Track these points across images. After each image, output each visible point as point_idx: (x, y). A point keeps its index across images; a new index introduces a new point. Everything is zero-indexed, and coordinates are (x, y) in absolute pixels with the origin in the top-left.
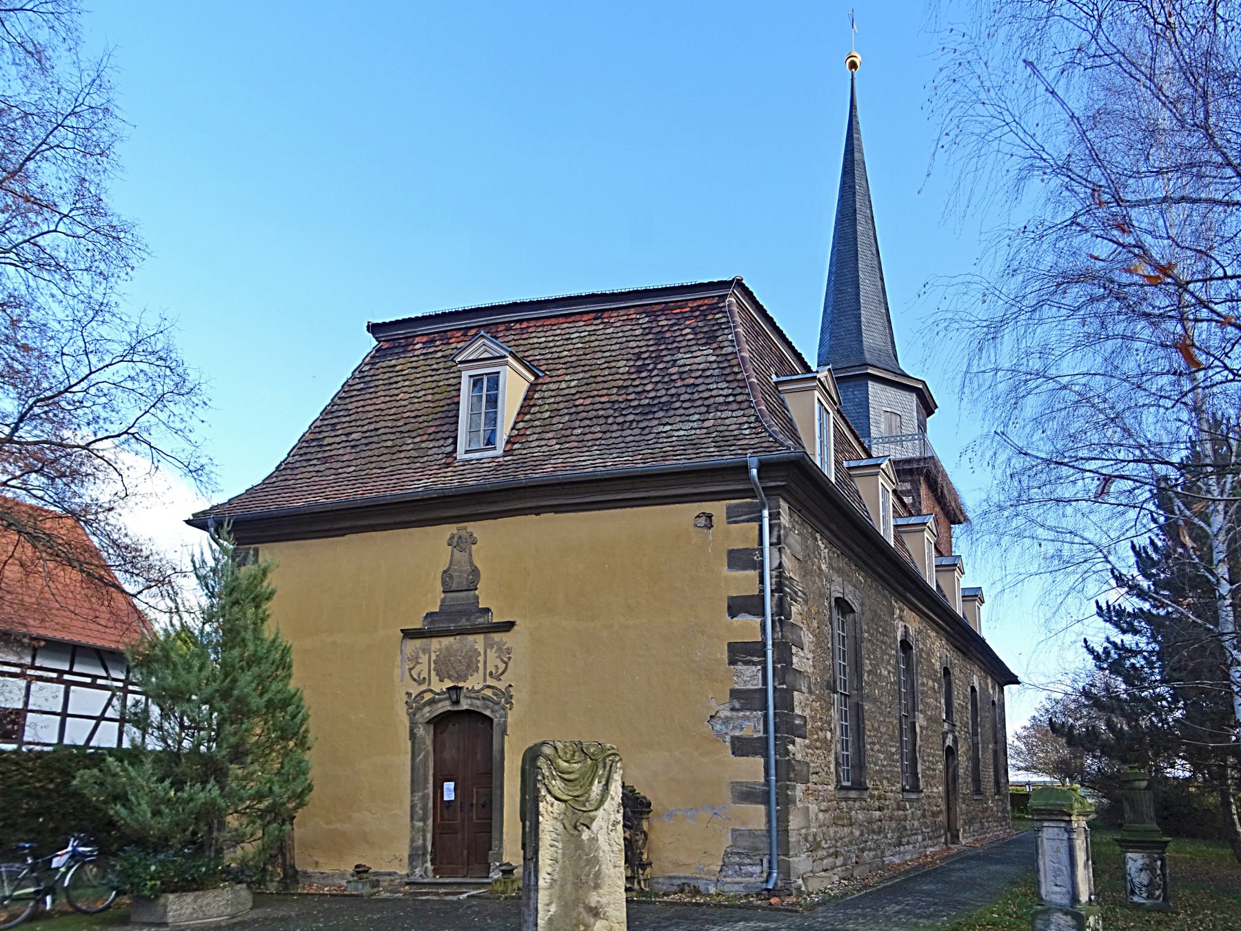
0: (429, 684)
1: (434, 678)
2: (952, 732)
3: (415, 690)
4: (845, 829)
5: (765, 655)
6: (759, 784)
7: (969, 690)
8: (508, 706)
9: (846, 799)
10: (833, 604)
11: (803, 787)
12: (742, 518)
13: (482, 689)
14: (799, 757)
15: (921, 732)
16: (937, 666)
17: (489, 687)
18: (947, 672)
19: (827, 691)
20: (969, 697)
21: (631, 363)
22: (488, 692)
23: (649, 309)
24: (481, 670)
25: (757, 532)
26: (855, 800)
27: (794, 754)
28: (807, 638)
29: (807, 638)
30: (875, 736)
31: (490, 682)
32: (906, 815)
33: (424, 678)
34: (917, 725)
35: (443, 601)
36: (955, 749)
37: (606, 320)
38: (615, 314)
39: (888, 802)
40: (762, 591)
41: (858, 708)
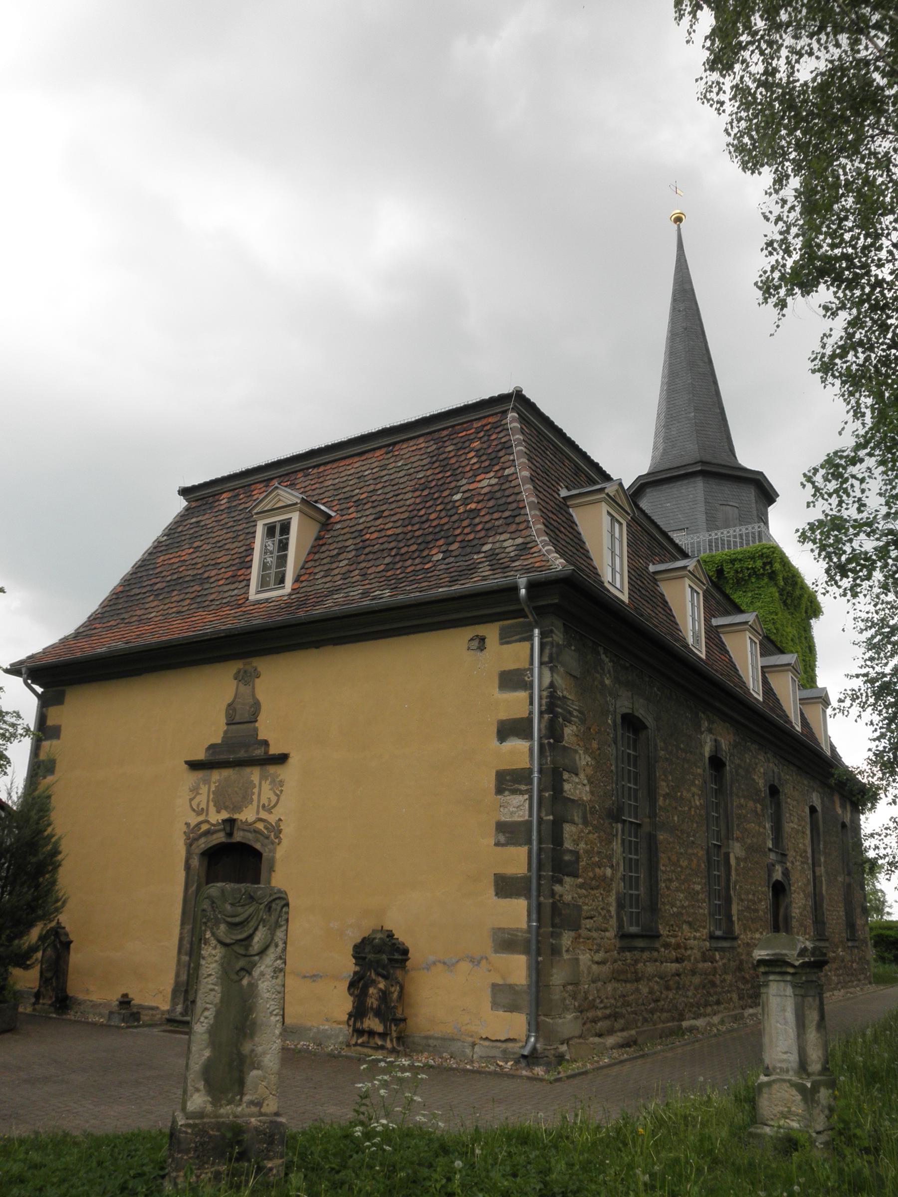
0: (207, 814)
1: (212, 809)
2: (782, 862)
3: (194, 820)
4: (629, 985)
5: (531, 783)
6: (521, 930)
7: (807, 810)
8: (277, 841)
9: (631, 949)
10: (619, 720)
11: (572, 934)
12: (514, 638)
13: (255, 822)
14: (568, 898)
15: (738, 864)
16: (761, 783)
17: (261, 820)
18: (774, 791)
19: (607, 822)
20: (808, 819)
21: (418, 493)
22: (260, 826)
23: (436, 435)
24: (255, 803)
25: (528, 651)
26: (643, 950)
27: (561, 896)
28: (583, 760)
29: (583, 760)
30: (673, 871)
31: (263, 815)
32: (715, 968)
33: (202, 809)
34: (732, 856)
35: (226, 732)
36: (786, 884)
37: (397, 453)
38: (404, 446)
39: (689, 952)
40: (531, 713)
41: (651, 839)
